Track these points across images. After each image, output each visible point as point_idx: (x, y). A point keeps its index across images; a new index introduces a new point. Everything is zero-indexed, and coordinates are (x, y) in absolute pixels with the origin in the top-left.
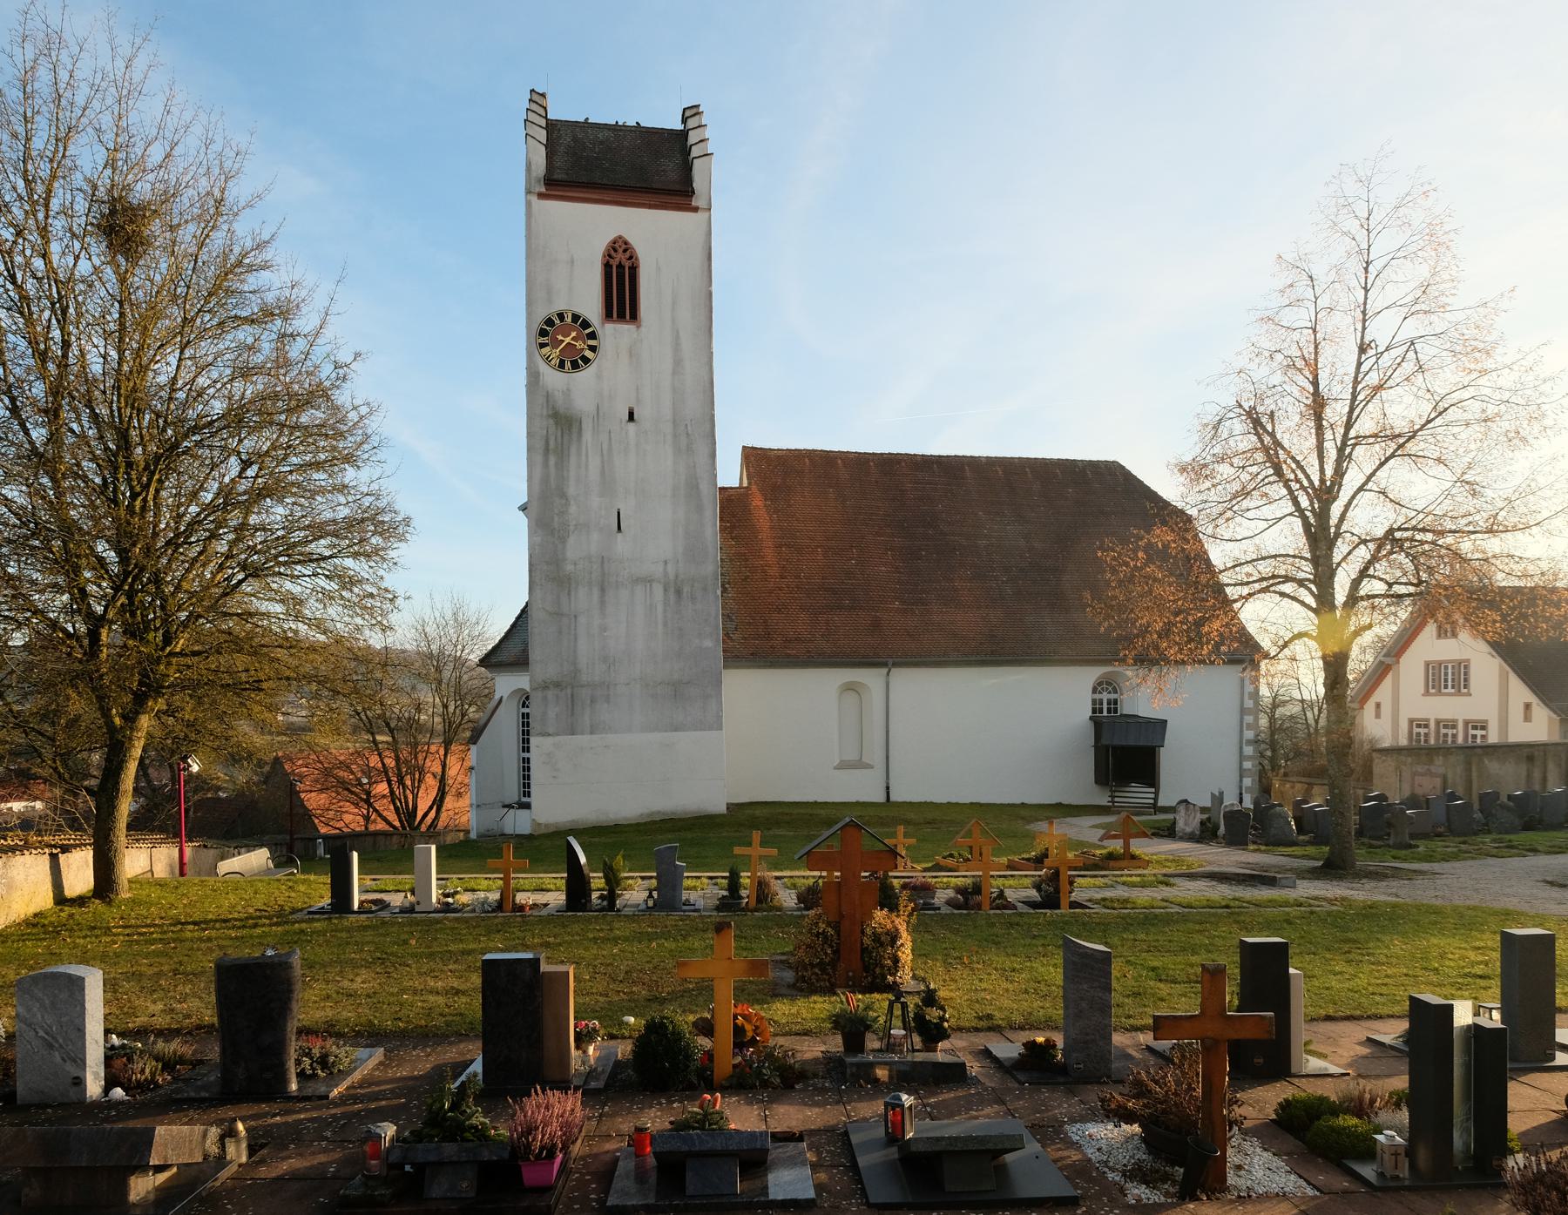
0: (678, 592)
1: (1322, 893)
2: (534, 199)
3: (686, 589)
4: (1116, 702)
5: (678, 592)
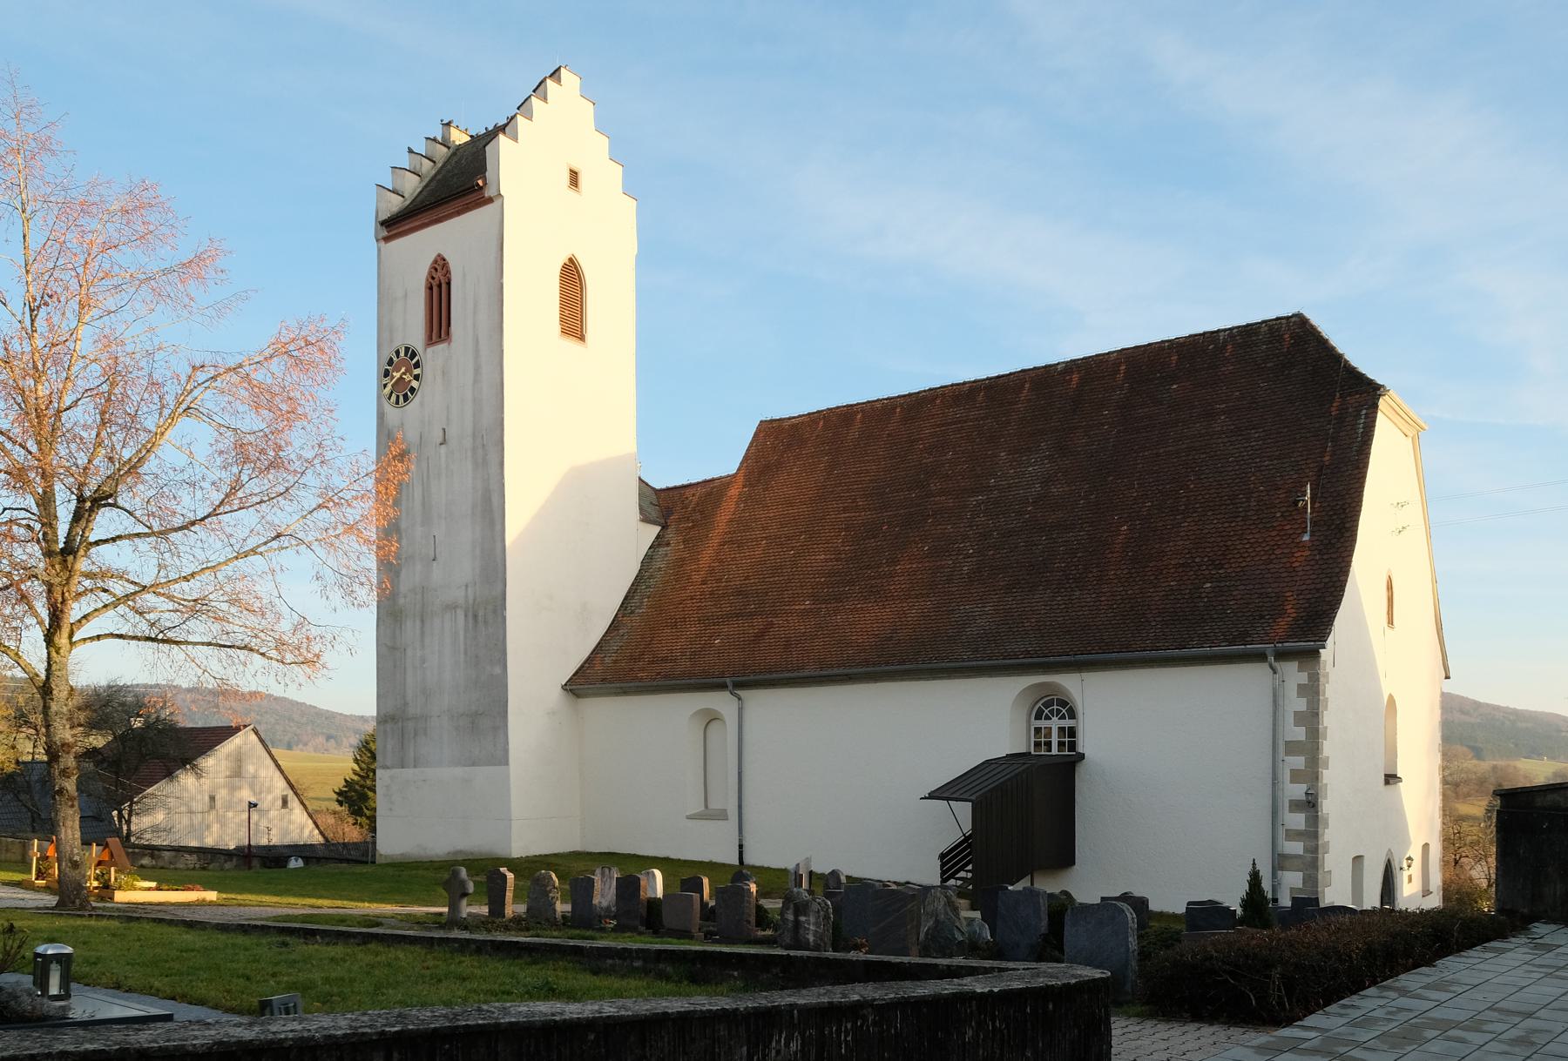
0: (475, 617)
1: (612, 944)
2: (382, 244)
3: (481, 613)
4: (1072, 732)
5: (475, 617)
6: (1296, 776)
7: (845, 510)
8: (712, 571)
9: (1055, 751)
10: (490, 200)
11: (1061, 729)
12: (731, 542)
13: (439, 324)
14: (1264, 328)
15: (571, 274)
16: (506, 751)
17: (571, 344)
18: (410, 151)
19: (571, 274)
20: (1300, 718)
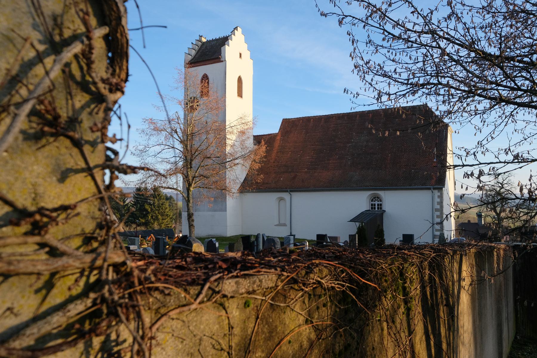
4: (381, 205)
6: (438, 217)
7: (312, 145)
8: (276, 159)
9: (376, 209)
10: (222, 61)
11: (378, 205)
12: (280, 152)
13: (204, 93)
14: (417, 107)
15: (240, 80)
16: (226, 208)
17: (239, 98)
18: (192, 43)
19: (240, 80)
20: (438, 203)
